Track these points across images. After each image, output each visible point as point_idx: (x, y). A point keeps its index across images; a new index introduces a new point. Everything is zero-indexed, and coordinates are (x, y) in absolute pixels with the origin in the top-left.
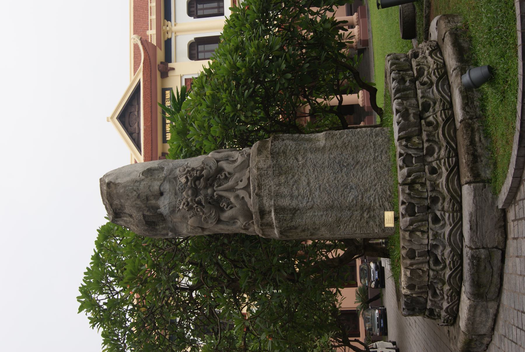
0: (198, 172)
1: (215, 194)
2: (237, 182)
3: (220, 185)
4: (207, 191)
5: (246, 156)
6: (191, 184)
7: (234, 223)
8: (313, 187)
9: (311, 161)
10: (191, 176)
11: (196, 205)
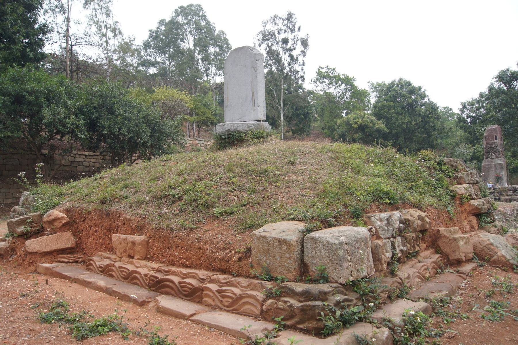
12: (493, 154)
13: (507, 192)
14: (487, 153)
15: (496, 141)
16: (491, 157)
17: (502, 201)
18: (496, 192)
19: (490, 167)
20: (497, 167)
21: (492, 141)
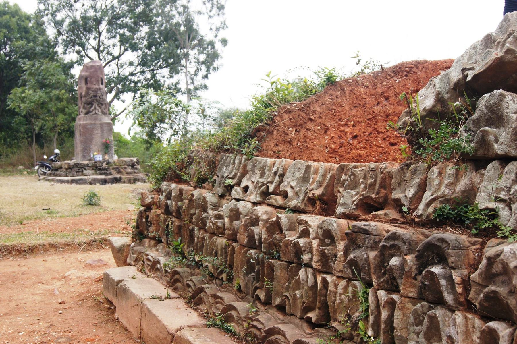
12: (97, 107)
13: (125, 168)
14: (88, 104)
15: (101, 86)
16: (94, 112)
17: (124, 182)
18: (111, 168)
19: (94, 128)
20: (104, 128)
21: (97, 86)
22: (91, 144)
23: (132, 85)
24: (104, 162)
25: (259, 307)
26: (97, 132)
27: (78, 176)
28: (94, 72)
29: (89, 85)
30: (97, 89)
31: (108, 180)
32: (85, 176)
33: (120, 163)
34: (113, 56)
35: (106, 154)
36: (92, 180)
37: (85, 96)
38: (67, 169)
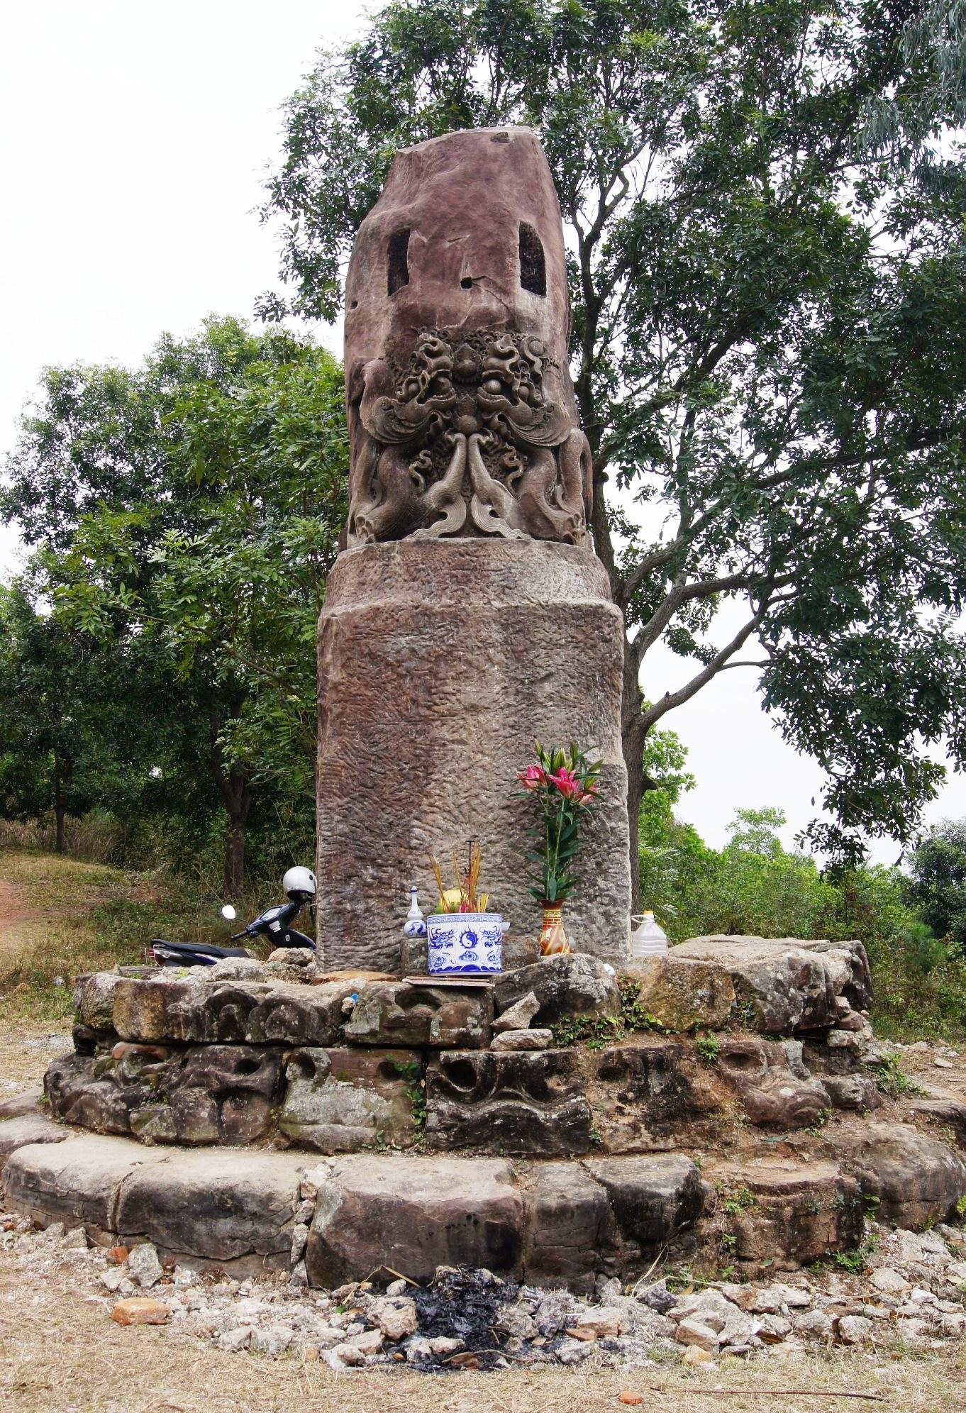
0: (524, 389)
1: (460, 436)
2: (489, 502)
3: (483, 450)
4: (469, 414)
5: (567, 532)
6: (493, 367)
7: (372, 489)
8: (461, 722)
9: (539, 720)
10: (513, 367)
11: (428, 377)
12: (483, 474)
13: (742, 1058)
15: (524, 301)
16: (455, 517)
18: (584, 1055)
19: (448, 656)
20: (544, 661)
21: (486, 300)
22: (409, 805)
23: (780, 420)
24: (513, 989)
25: (879, 1050)
26: (470, 692)
27: (228, 1136)
28: (466, 178)
29: (419, 291)
30: (487, 317)
31: (536, 1233)
32: (301, 1145)
33: (683, 1008)
34: (703, 656)
35: (546, 903)
36: (343, 1220)
37: (382, 387)
38: (146, 1052)
